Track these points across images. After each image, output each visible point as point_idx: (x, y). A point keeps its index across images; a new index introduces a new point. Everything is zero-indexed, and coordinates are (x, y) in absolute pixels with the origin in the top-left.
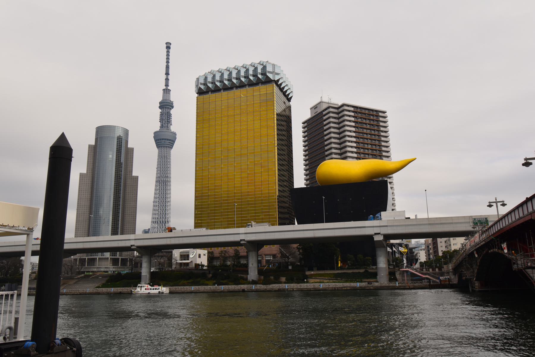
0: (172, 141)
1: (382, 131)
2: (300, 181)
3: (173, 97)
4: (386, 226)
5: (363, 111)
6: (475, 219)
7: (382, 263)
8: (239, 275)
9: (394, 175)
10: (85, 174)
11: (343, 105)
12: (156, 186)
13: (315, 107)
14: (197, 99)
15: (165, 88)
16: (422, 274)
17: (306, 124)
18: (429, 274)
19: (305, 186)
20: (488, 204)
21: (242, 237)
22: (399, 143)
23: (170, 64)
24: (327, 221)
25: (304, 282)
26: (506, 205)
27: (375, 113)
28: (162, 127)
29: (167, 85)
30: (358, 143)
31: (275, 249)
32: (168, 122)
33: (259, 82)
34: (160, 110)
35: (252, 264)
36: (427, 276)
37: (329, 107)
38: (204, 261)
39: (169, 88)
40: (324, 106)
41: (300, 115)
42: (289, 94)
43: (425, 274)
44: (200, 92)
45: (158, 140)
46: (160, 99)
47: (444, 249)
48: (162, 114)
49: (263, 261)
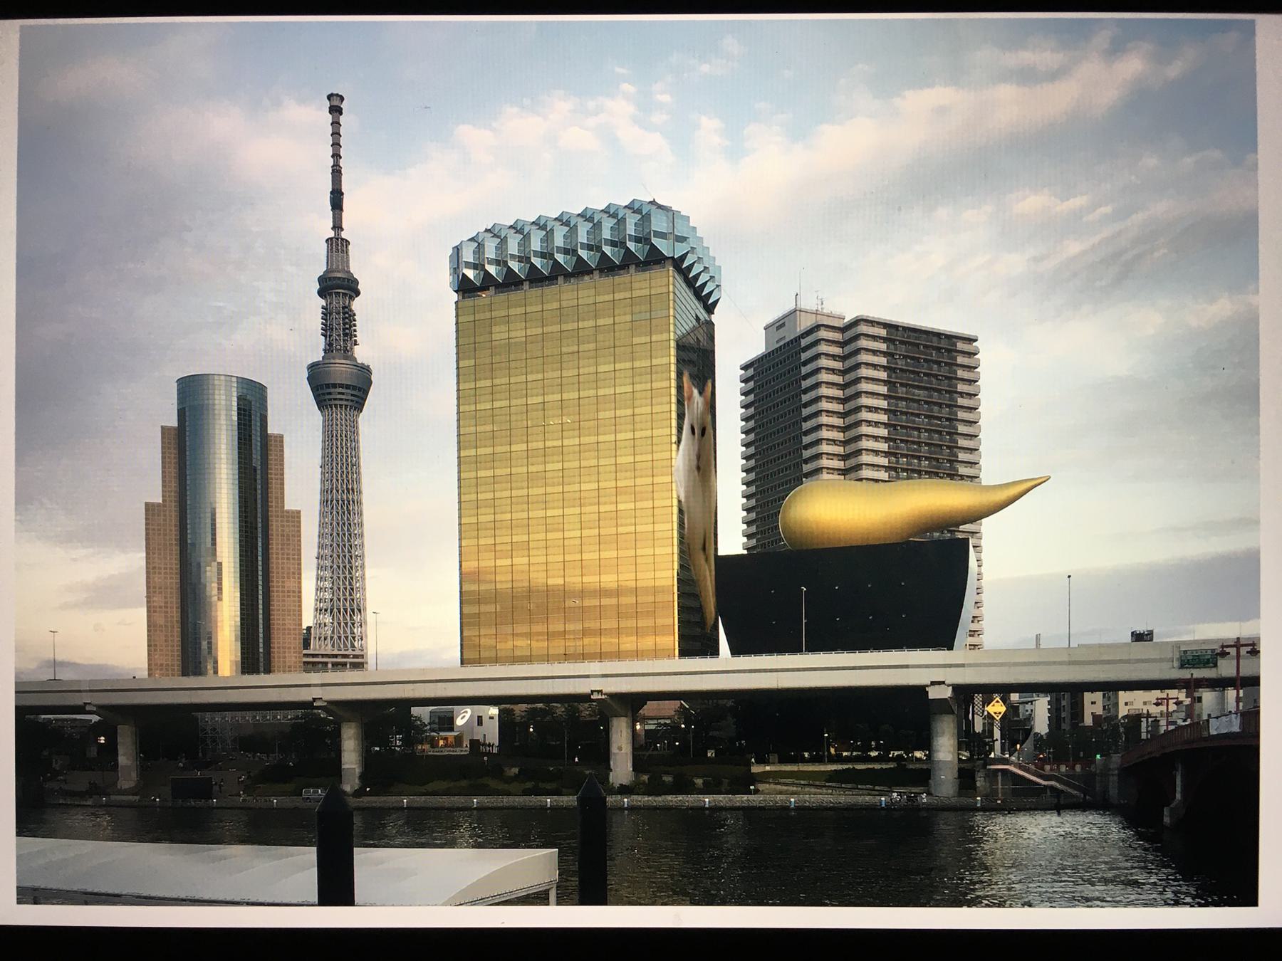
0: (360, 389)
1: (961, 394)
3: (357, 268)
4: (963, 665)
6: (1185, 652)
7: (946, 748)
11: (856, 322)
12: (322, 514)
13: (779, 324)
14: (457, 308)
15: (332, 234)
17: (751, 372)
19: (745, 552)
21: (316, 693)
23: (342, 163)
25: (749, 792)
28: (329, 349)
29: (337, 226)
30: (894, 412)
31: (670, 707)
32: (346, 335)
33: (629, 261)
34: (323, 302)
35: (620, 749)
36: (1053, 783)
38: (491, 733)
39: (344, 235)
40: (805, 323)
41: (738, 343)
42: (710, 293)
44: (465, 288)
45: (321, 387)
46: (321, 269)
47: (1099, 710)
48: (327, 313)
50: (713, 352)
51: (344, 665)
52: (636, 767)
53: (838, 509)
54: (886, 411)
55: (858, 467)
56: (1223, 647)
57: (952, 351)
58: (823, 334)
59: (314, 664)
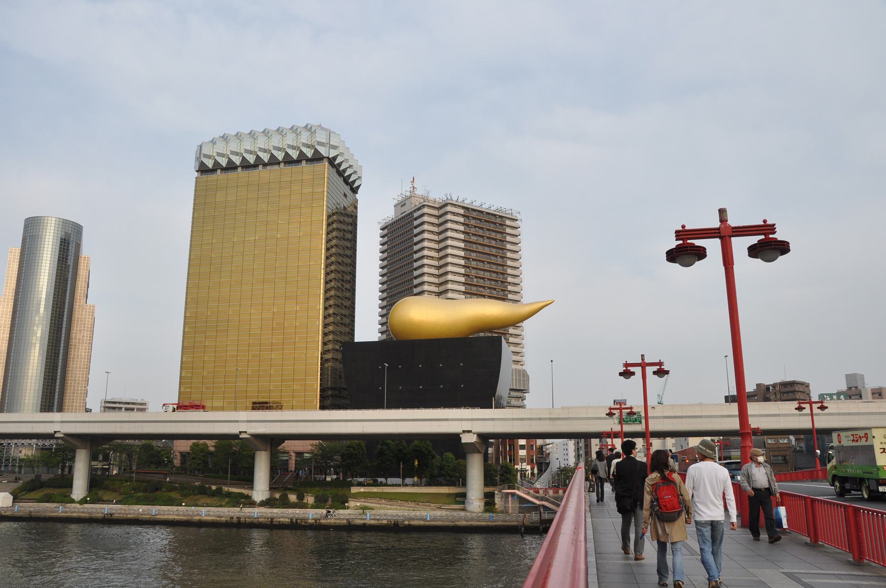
2: (367, 328)
5: (493, 219)
8: (226, 489)
9: (526, 324)
16: (537, 498)
17: (386, 231)
18: (547, 500)
19: (384, 337)
20: (622, 369)
21: (242, 427)
22: (537, 268)
24: (390, 406)
26: (667, 372)
27: (499, 220)
36: (544, 503)
37: (424, 206)
40: (416, 203)
42: (354, 181)
43: (542, 499)
44: (203, 170)
49: (290, 462)
50: (354, 217)
51: (132, 409)
52: (272, 488)
53: (431, 313)
55: (446, 291)
58: (426, 210)
59: (114, 408)
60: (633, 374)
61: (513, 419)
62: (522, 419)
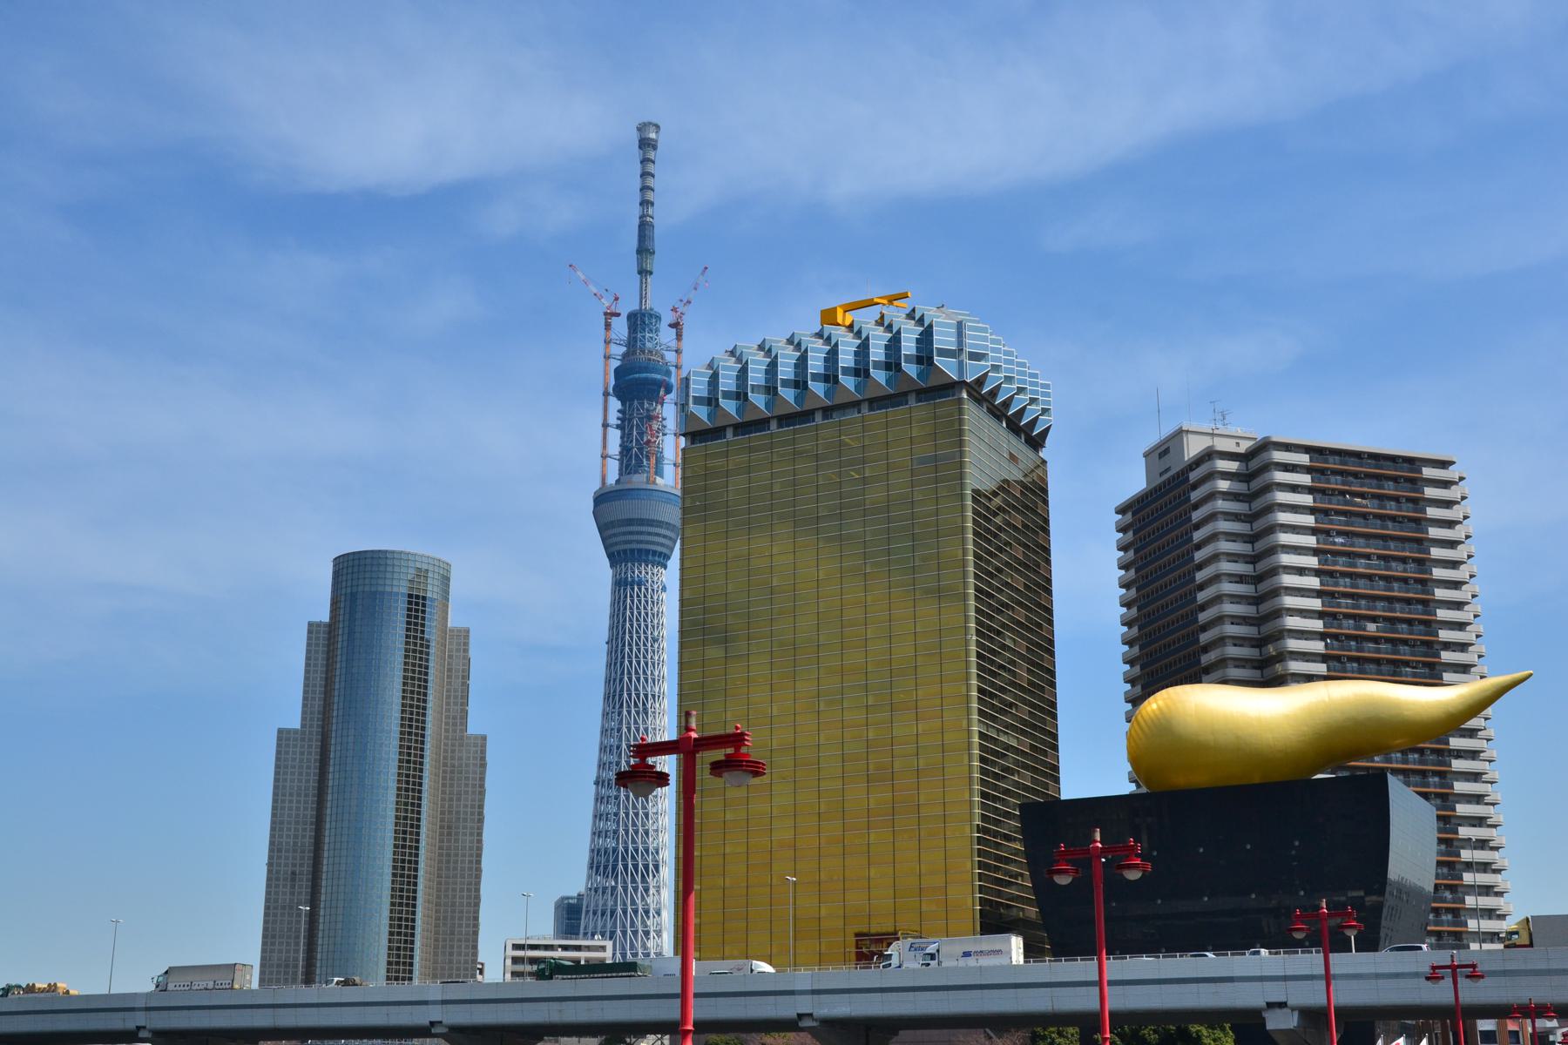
10: (295, 731)
20: (626, 762)
45: (612, 524)
54: (1317, 573)
56: (1434, 968)
57: (1416, 483)
60: (662, 779)
61: (1378, 976)
62: (1397, 976)
